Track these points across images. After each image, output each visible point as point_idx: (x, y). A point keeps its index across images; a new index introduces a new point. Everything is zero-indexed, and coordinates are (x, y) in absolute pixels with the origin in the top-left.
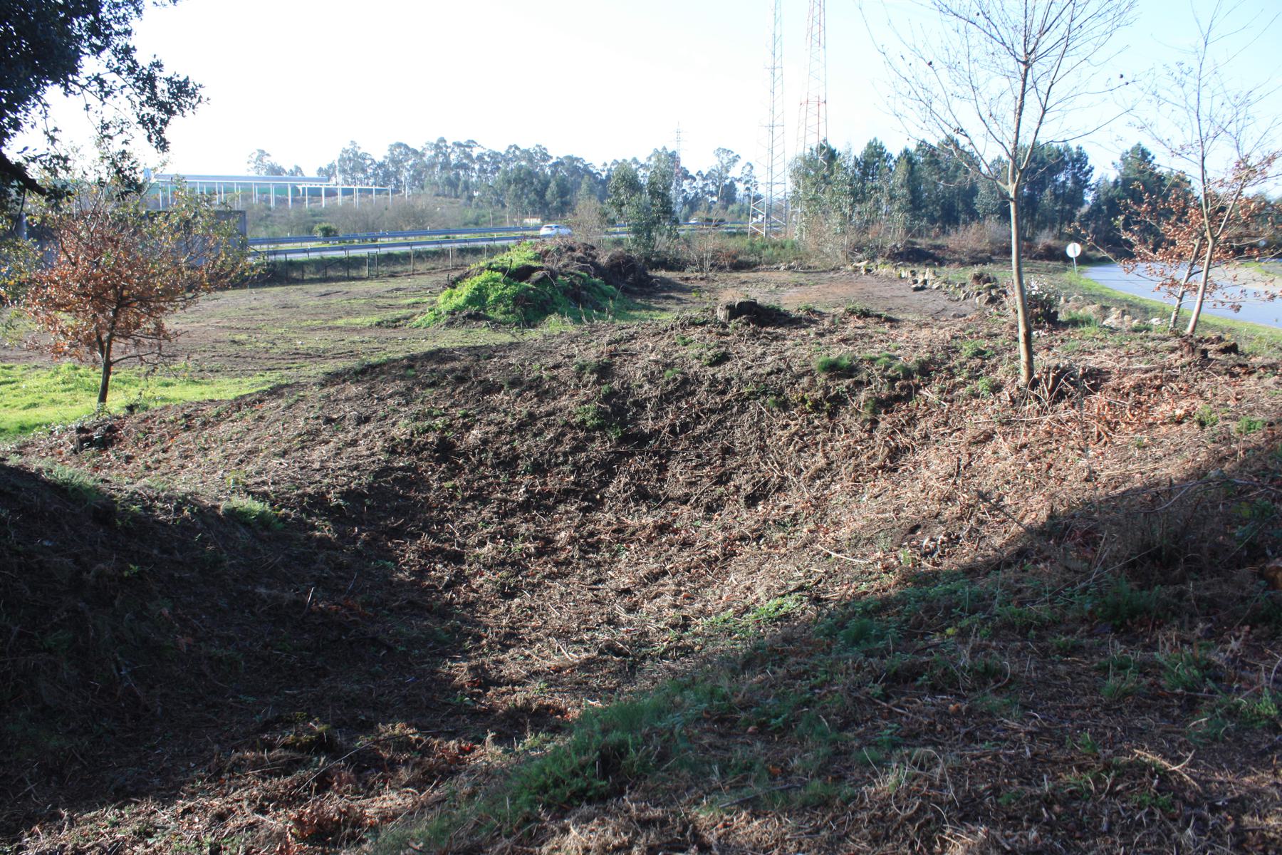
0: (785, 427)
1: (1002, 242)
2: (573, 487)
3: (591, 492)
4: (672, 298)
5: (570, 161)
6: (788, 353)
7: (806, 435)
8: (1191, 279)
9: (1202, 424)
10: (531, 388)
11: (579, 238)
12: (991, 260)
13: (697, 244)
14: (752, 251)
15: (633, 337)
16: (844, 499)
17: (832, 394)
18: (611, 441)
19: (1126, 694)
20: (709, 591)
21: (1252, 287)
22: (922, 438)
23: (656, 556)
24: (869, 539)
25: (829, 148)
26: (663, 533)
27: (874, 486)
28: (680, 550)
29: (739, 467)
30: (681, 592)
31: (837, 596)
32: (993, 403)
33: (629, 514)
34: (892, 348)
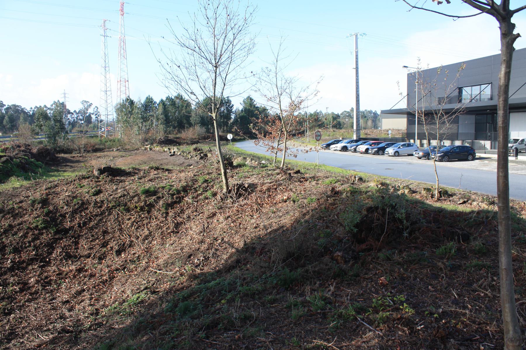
0: (129, 219)
1: (202, 135)
2: (35, 257)
3: (44, 258)
4: (68, 166)
5: (14, 107)
6: (127, 188)
7: (138, 222)
8: (279, 147)
9: (294, 201)
10: (9, 213)
11: (22, 141)
12: (199, 142)
13: (77, 142)
14: (101, 144)
15: (56, 186)
16: (158, 247)
17: (148, 203)
18: (51, 233)
19: (300, 317)
20: (105, 295)
21: (300, 148)
22: (187, 218)
23: (79, 283)
24: (172, 263)
25: (130, 100)
26: (80, 272)
27: (171, 240)
28: (89, 279)
29: (111, 239)
30: (92, 298)
31: (163, 289)
32: (214, 201)
33: (63, 266)
34: (170, 182)
